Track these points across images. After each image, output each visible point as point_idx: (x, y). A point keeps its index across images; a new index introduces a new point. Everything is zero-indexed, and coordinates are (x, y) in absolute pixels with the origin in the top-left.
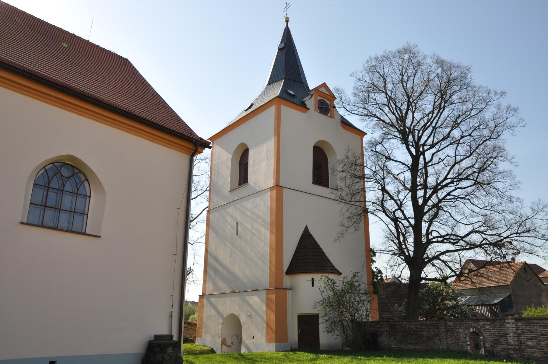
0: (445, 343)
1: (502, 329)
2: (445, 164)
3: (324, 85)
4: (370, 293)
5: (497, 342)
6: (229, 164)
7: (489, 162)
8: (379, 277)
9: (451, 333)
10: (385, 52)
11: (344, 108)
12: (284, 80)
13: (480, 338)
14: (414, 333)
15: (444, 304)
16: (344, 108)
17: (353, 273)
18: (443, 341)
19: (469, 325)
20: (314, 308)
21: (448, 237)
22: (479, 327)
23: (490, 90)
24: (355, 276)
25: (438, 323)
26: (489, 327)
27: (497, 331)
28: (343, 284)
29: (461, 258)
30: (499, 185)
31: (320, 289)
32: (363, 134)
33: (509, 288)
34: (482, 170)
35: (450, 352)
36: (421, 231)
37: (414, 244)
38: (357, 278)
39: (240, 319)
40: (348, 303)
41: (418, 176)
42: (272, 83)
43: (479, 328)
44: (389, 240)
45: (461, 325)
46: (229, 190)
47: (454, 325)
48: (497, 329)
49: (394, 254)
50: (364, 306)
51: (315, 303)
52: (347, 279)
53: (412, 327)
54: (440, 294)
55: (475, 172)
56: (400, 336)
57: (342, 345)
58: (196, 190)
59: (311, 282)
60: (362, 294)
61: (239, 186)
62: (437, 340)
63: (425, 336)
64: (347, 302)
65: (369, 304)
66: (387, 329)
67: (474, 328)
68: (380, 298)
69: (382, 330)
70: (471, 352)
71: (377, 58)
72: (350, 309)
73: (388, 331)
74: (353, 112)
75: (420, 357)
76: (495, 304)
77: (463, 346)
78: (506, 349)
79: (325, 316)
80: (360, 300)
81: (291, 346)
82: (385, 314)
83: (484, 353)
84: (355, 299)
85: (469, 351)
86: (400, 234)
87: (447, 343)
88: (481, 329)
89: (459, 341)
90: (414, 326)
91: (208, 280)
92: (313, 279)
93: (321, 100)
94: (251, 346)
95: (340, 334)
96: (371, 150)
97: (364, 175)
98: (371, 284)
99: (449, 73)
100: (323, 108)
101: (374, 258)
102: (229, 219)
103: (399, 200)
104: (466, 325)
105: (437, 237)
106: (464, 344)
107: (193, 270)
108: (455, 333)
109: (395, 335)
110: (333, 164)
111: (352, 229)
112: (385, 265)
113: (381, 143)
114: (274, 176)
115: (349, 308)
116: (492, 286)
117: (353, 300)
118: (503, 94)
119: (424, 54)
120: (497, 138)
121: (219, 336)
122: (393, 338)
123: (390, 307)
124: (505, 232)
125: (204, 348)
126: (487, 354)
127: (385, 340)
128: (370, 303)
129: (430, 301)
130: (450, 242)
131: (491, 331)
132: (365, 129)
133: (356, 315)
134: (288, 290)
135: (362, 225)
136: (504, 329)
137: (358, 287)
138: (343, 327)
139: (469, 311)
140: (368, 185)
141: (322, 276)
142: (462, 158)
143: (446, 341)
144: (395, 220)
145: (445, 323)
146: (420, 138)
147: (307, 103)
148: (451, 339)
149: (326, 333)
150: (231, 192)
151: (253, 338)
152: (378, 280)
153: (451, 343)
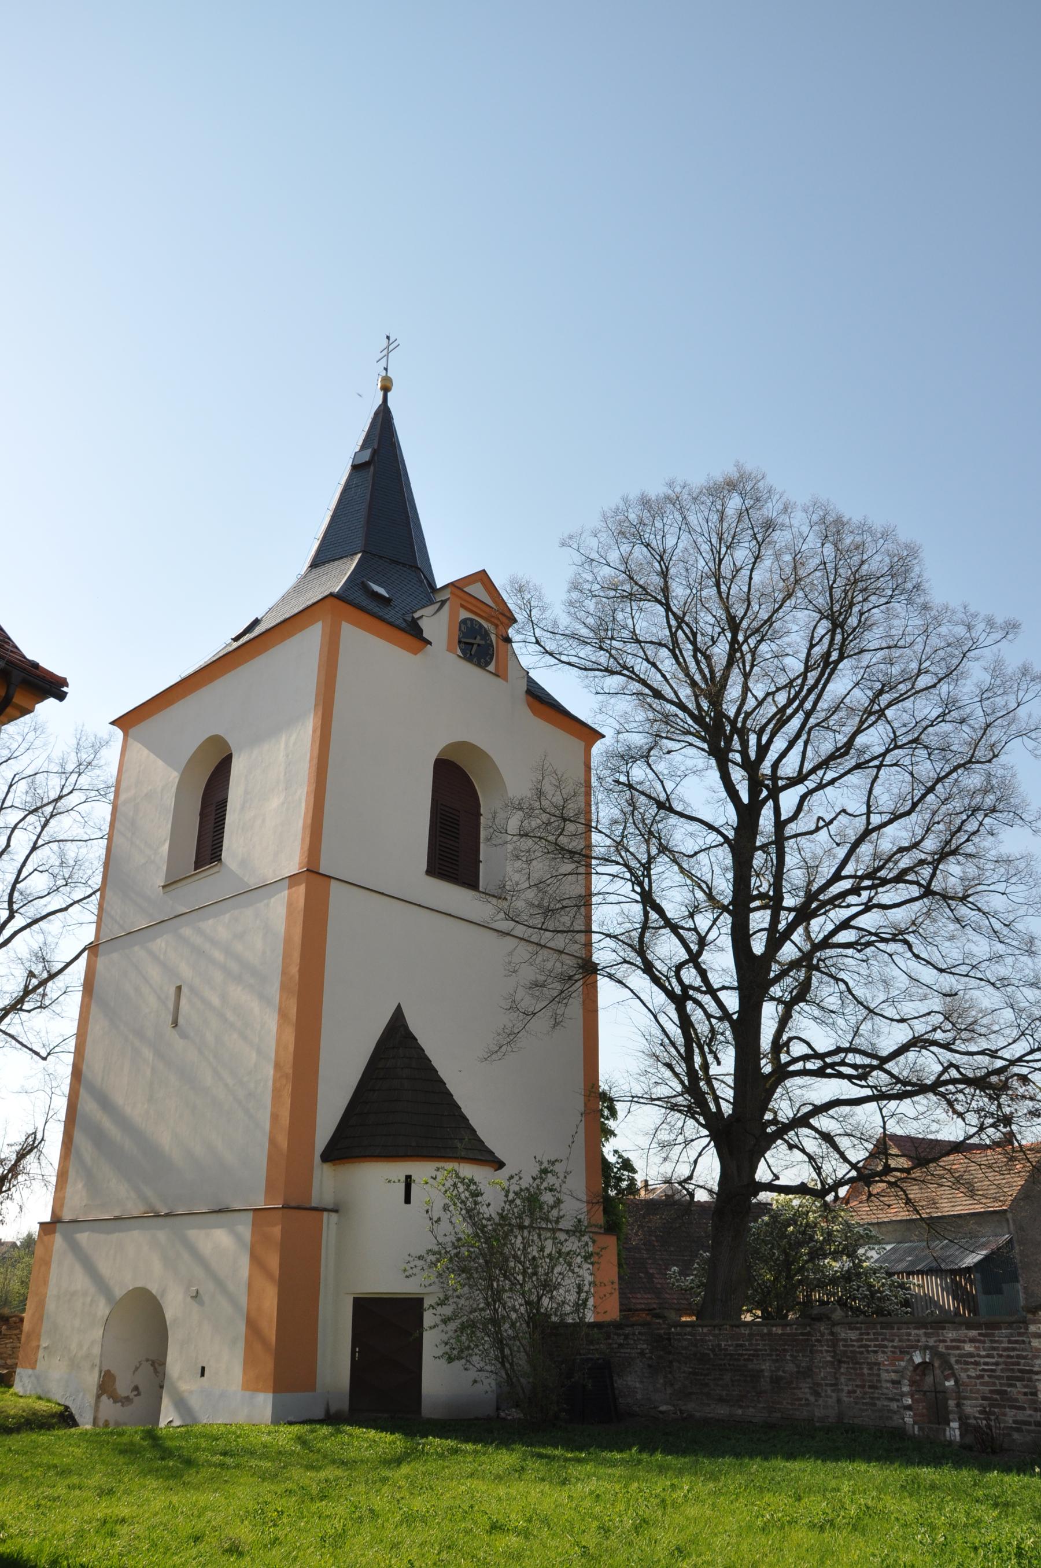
0: (831, 1401)
1: (1019, 1357)
2: (834, 837)
3: (482, 577)
4: (593, 1229)
5: (1000, 1399)
6: (169, 800)
7: (972, 826)
8: (624, 1180)
9: (851, 1366)
10: (670, 485)
11: (538, 642)
12: (359, 555)
13: (947, 1384)
14: (729, 1365)
15: (819, 1269)
16: (538, 642)
17: (541, 1163)
18: (823, 1394)
19: (909, 1340)
20: (407, 1277)
21: (837, 1059)
22: (942, 1348)
23: (974, 616)
24: (545, 1171)
25: (809, 1334)
26: (975, 1347)
27: (1000, 1360)
28: (507, 1196)
29: (886, 1119)
30: (995, 902)
31: (427, 1211)
32: (592, 735)
33: (1007, 1220)
34: (943, 855)
35: (847, 1432)
36: (760, 1039)
37: (735, 1081)
38: (551, 1180)
39: (163, 1306)
40: (520, 1262)
41: (753, 873)
42: (324, 563)
43: (943, 1350)
44: (659, 1063)
45: (883, 1340)
46: (162, 884)
47: (861, 1340)
48: (1001, 1356)
49: (674, 1107)
50: (570, 1274)
51: (411, 1259)
52: (521, 1182)
53: (723, 1344)
54: (806, 1232)
55: (922, 862)
56: (684, 1372)
57: (497, 1402)
58: (66, 885)
59: (403, 1186)
60: (567, 1232)
61: (195, 869)
62: (804, 1390)
63: (766, 1374)
64: (515, 1257)
65: (590, 1266)
66: (643, 1350)
67: (928, 1352)
68: (625, 1246)
69: (629, 1353)
70: (916, 1432)
71: (645, 503)
72: (524, 1279)
73: (647, 1356)
74: (564, 658)
75: (752, 1456)
76: (968, 1269)
77: (890, 1411)
78: (1028, 1423)
79: (442, 1303)
80: (560, 1252)
81: (328, 1405)
82: (639, 1296)
83: (958, 1438)
84: (542, 1249)
85: (909, 1428)
86: (694, 1045)
87: (839, 1401)
88: (949, 1354)
89: (876, 1395)
90: (730, 1343)
91: (72, 1173)
92: (408, 1178)
93: (469, 622)
94: (195, 1402)
95: (488, 1368)
96: (614, 781)
97: (589, 846)
98: (598, 1202)
99: (856, 560)
100: (475, 647)
101: (611, 1124)
102: (154, 973)
103: (695, 929)
104: (900, 1341)
105: (805, 1058)
106: (894, 1405)
107: (43, 1140)
108: (865, 1366)
109: (668, 1370)
110: (493, 811)
111: (541, 1024)
112: (644, 1142)
113: (646, 757)
114: (303, 839)
115: (520, 1278)
116: (968, 1214)
117: (535, 1253)
118: (1011, 628)
119: (784, 499)
120: (989, 761)
121: (93, 1366)
122: (661, 1381)
123: (657, 1276)
124: (1010, 1044)
125: (42, 1406)
126: (969, 1439)
127: (638, 1385)
128: (592, 1263)
129: (778, 1259)
130: (840, 1075)
131: (982, 1360)
132: (600, 717)
133: (545, 1301)
134: (325, 1214)
135: (575, 1007)
136: (1024, 1354)
137: (552, 1207)
138: (499, 1342)
139: (891, 1291)
140: (598, 883)
141: (438, 1169)
142: (886, 818)
143: (834, 1395)
144: (680, 1000)
145: (832, 1333)
146: (763, 750)
147: (424, 624)
148: (850, 1388)
149: (443, 1361)
150: (168, 889)
151: (203, 1375)
152: (620, 1191)
153: (852, 1399)
